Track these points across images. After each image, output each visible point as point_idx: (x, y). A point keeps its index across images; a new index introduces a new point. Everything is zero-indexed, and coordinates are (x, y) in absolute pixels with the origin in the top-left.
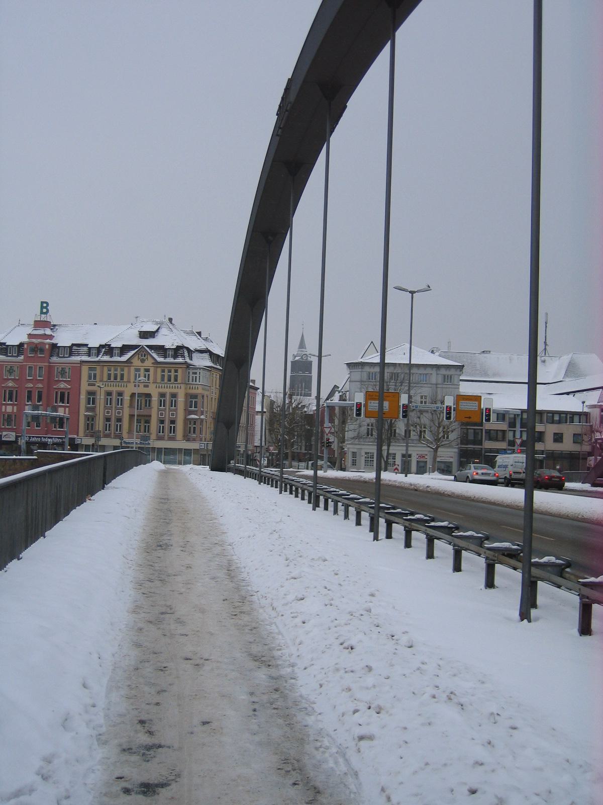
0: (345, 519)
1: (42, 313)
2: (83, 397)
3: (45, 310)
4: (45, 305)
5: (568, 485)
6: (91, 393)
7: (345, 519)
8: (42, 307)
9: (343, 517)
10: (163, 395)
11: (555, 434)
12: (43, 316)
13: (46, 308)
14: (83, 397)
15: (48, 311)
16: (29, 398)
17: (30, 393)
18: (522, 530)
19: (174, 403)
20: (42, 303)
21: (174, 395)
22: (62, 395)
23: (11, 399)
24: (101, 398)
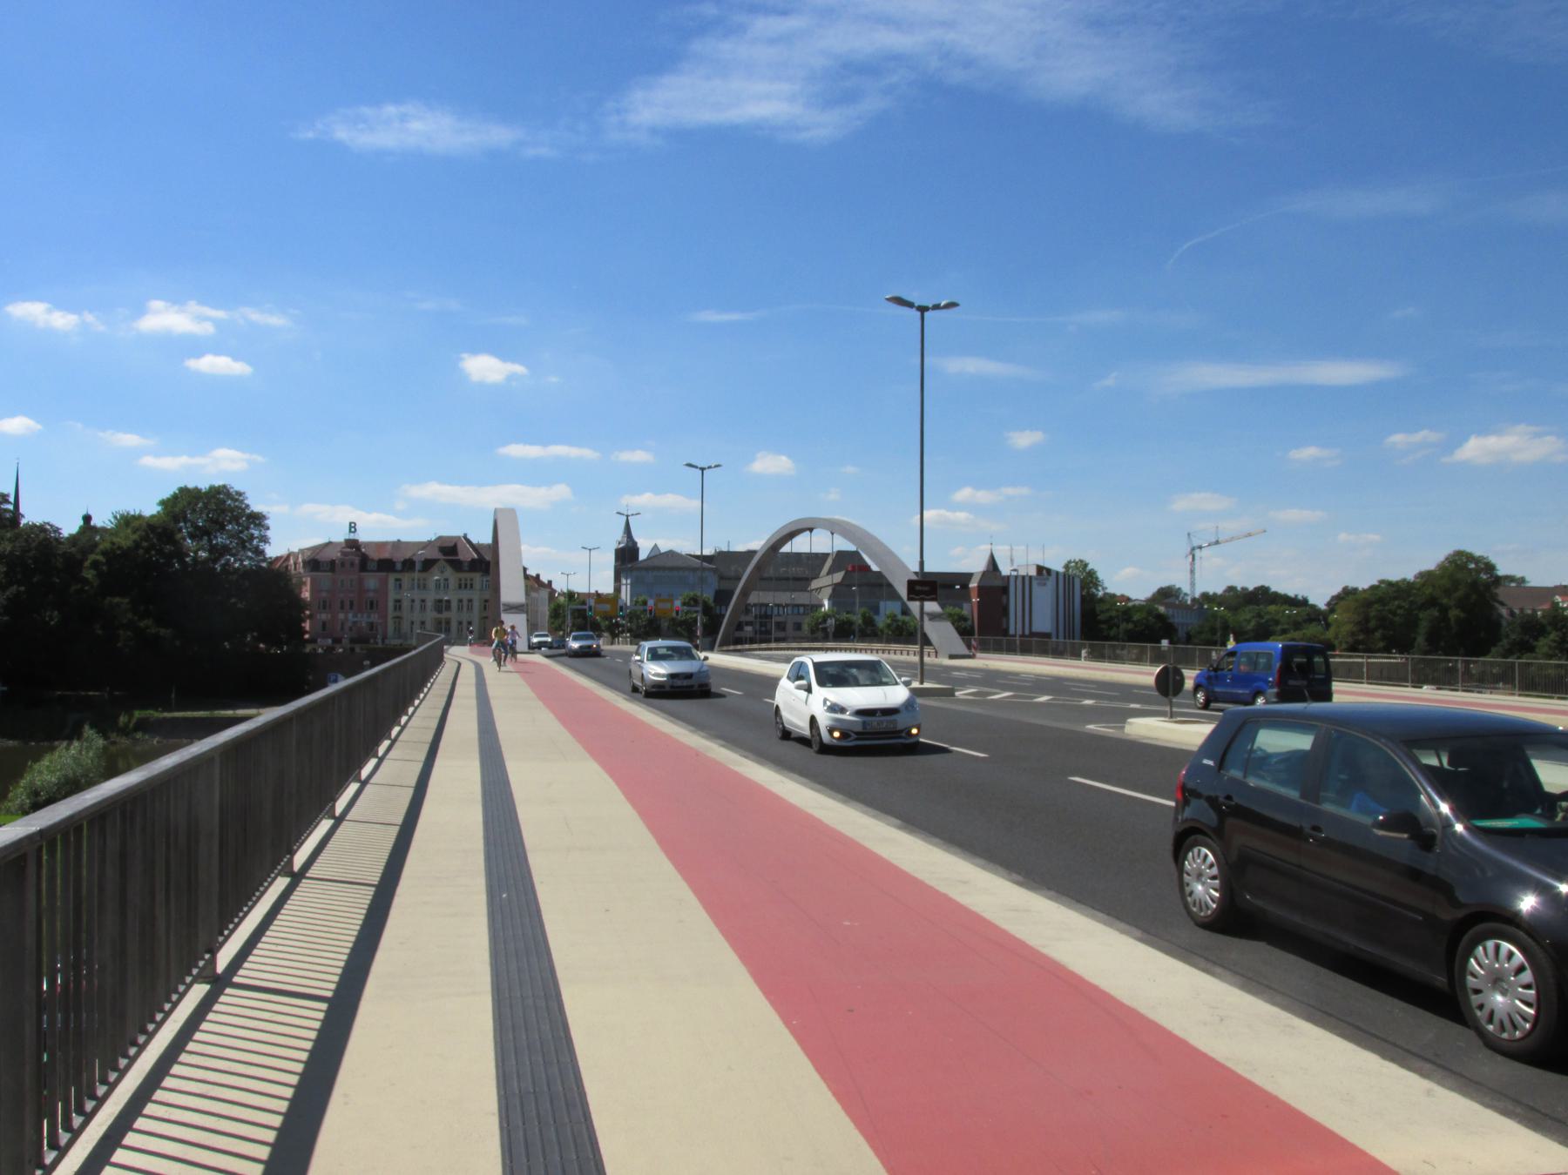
0: (656, 545)
1: (350, 531)
2: (391, 604)
3: (353, 530)
4: (353, 525)
5: (1005, 626)
6: (398, 601)
7: (656, 545)
8: (350, 527)
9: (1042, 564)
10: (461, 601)
11: (795, 624)
12: (352, 534)
13: (354, 527)
14: (391, 604)
15: (355, 530)
16: (342, 607)
17: (342, 602)
18: (1176, 712)
19: (470, 608)
20: (350, 523)
21: (470, 601)
22: (372, 603)
23: (324, 608)
24: (406, 604)
